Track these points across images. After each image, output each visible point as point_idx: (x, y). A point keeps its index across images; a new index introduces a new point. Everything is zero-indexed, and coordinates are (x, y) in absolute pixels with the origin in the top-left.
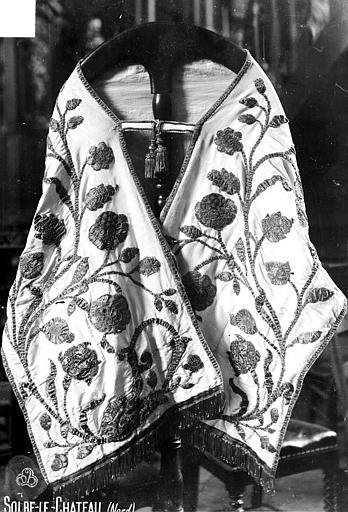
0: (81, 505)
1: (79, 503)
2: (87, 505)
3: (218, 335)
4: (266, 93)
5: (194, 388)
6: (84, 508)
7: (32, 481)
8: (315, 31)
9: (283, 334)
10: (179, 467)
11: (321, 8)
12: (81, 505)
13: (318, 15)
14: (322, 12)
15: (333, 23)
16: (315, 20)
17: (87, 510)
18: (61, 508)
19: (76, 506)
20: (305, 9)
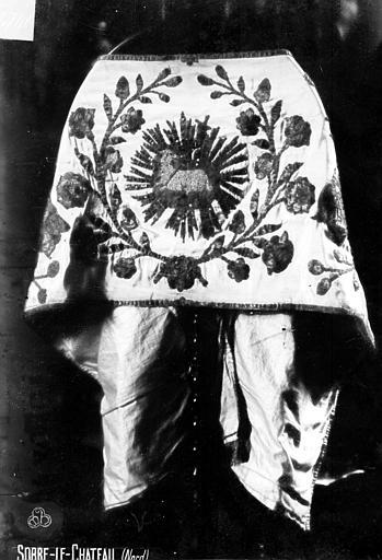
0: (96, 552)
1: (93, 549)
2: (102, 552)
3: (293, 373)
4: (226, 264)
5: (301, 168)
6: (99, 555)
7: (45, 520)
8: (342, 31)
9: (114, 113)
10: (177, 417)
11: (351, 8)
12: (96, 552)
13: (346, 15)
14: (351, 12)
15: (361, 27)
16: (343, 22)
17: (101, 557)
18: (77, 555)
19: (91, 552)
20: (334, 13)
